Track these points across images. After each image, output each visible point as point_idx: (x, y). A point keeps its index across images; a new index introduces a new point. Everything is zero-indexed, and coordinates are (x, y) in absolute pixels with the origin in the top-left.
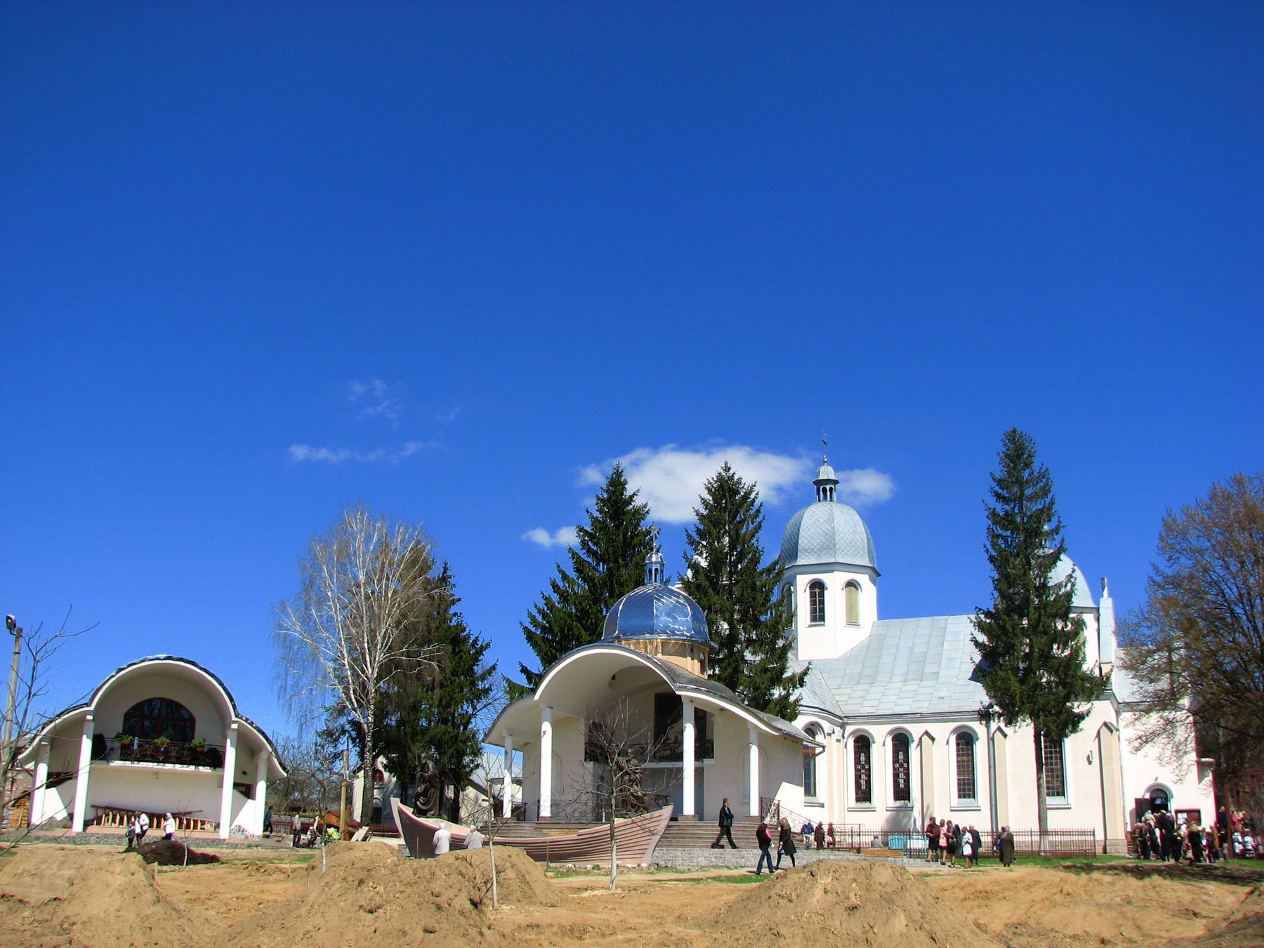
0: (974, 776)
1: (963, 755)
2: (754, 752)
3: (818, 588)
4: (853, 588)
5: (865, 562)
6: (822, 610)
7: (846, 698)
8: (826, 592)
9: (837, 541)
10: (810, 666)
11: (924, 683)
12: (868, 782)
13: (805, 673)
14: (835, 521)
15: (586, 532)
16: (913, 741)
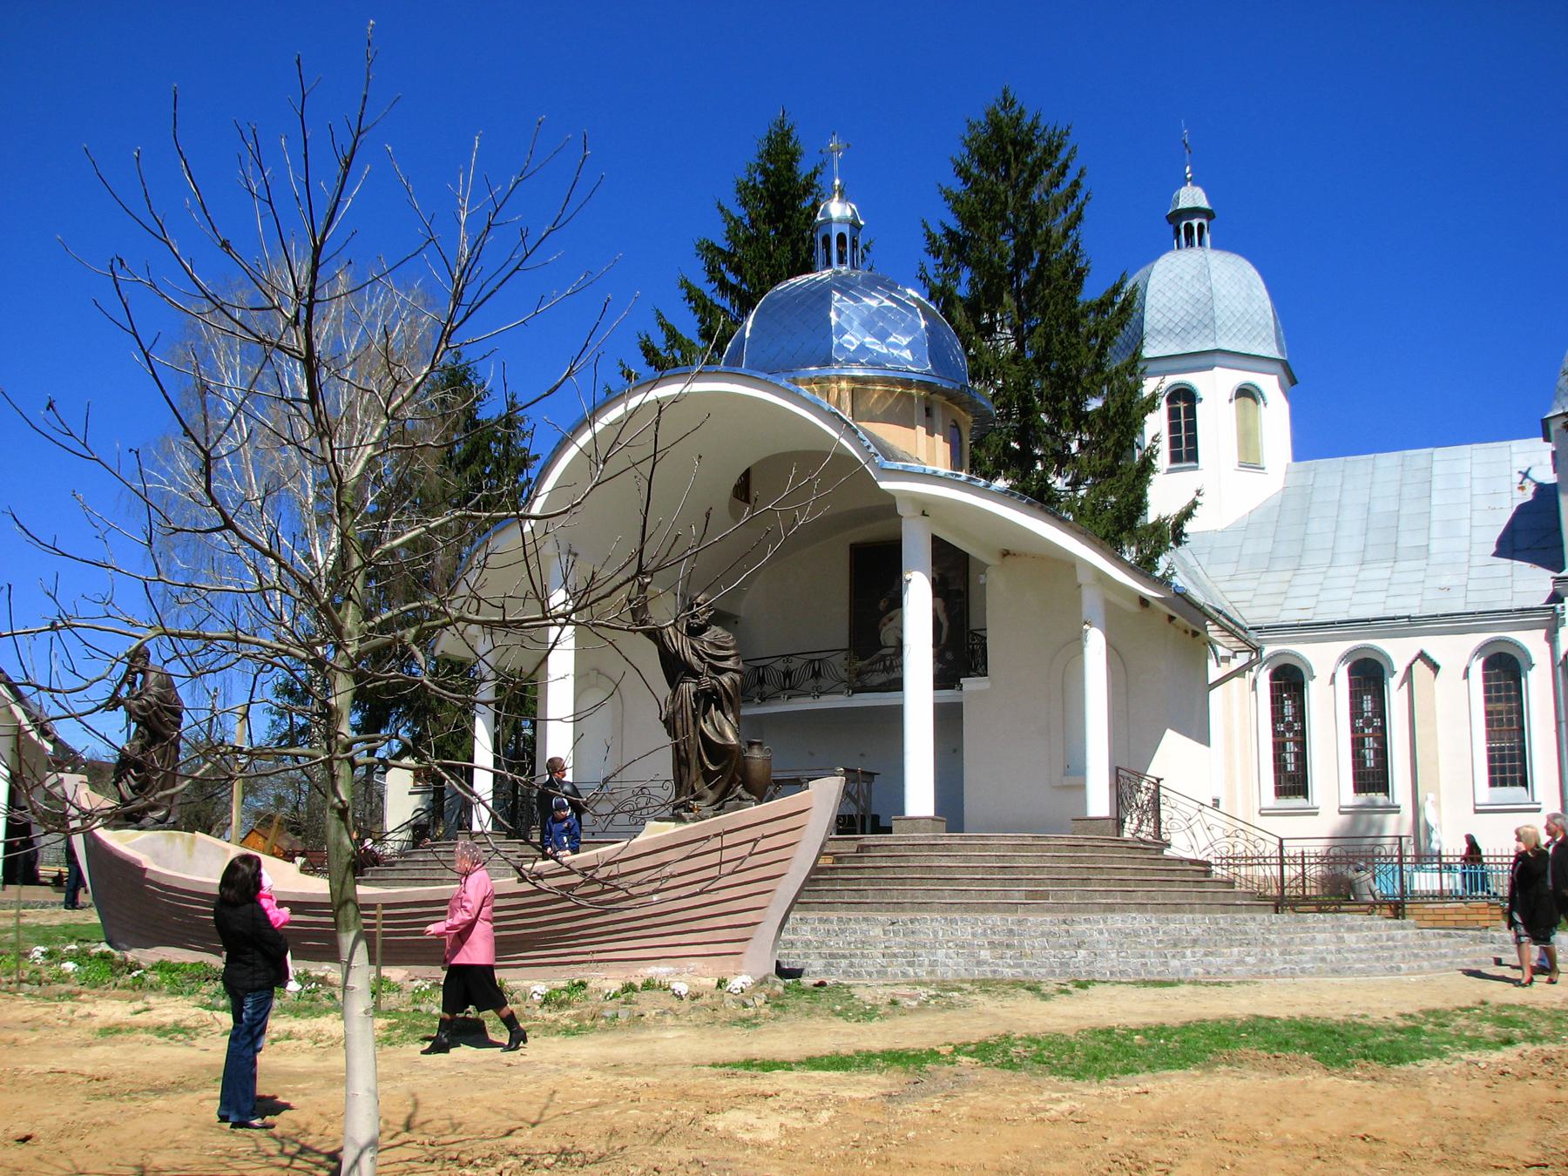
0: (1523, 740)
1: (1498, 699)
2: (1095, 644)
3: (1184, 399)
4: (1250, 401)
5: (1272, 351)
6: (1193, 441)
7: (1248, 596)
8: (1199, 407)
9: (1218, 312)
10: (1199, 499)
11: (1402, 565)
12: (1302, 757)
13: (1187, 514)
14: (1214, 276)
15: (721, 251)
16: (1393, 673)
